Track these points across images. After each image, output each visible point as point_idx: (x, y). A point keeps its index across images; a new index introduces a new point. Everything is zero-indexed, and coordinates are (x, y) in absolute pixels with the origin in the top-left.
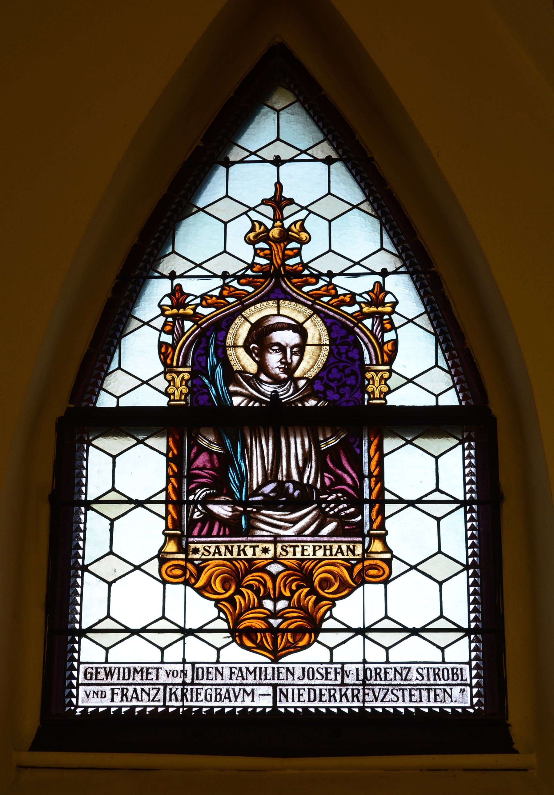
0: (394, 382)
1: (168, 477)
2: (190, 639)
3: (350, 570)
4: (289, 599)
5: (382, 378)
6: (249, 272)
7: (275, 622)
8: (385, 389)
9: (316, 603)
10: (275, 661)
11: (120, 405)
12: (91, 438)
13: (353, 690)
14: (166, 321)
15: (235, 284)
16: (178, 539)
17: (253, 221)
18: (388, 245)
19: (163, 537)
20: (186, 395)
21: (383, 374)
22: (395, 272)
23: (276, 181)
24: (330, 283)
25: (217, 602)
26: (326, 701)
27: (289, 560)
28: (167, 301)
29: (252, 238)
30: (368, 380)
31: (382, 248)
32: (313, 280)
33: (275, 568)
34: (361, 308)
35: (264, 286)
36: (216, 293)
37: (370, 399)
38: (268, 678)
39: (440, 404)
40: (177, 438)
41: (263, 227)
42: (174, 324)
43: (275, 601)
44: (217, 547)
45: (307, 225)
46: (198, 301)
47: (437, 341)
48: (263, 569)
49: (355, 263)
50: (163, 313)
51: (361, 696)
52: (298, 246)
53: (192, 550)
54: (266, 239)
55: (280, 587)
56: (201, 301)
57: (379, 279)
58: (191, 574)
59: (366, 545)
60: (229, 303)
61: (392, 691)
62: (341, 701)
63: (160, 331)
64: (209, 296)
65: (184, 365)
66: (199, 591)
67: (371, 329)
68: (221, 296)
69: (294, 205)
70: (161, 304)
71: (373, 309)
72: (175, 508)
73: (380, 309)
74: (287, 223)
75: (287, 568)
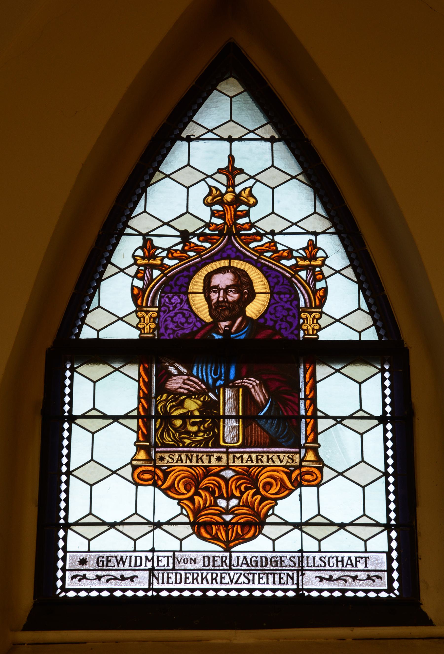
0: (324, 321)
1: (139, 398)
2: (158, 531)
3: (289, 475)
4: (239, 498)
5: (314, 318)
6: (207, 231)
7: (228, 518)
8: (317, 327)
9: (260, 503)
10: (228, 549)
11: (362, 339)
12: (75, 366)
13: (212, 574)
14: (138, 269)
15: (195, 240)
16: (147, 450)
17: (210, 187)
18: (320, 210)
19: (135, 448)
20: (154, 329)
21: (315, 315)
22: (324, 232)
23: (229, 154)
24: (273, 241)
25: (180, 502)
26: (264, 584)
27: (237, 467)
28: (140, 253)
29: (209, 201)
30: (304, 319)
31: (315, 212)
32: (259, 238)
33: (228, 474)
34: (297, 262)
35: (218, 243)
36: (180, 247)
37: (305, 334)
38: (309, 565)
39: (362, 339)
40: (147, 367)
41: (218, 192)
42: (145, 273)
43: (228, 500)
44: (180, 456)
45: (254, 192)
46: (164, 254)
47: (360, 288)
48: (217, 474)
49: (293, 224)
50: (135, 263)
51: (219, 579)
52: (246, 208)
53: (159, 458)
54: (221, 203)
55: (232, 490)
56: (168, 254)
57: (313, 238)
58: (159, 478)
59: (302, 455)
60: (190, 257)
61: (249, 581)
62: (202, 583)
63: (133, 277)
64: (173, 250)
65: (153, 305)
66: (164, 491)
67: (305, 279)
68: (183, 251)
69: (244, 174)
70: (136, 254)
71: (307, 263)
72: (144, 423)
73: (313, 263)
74: (238, 190)
75: (237, 473)
